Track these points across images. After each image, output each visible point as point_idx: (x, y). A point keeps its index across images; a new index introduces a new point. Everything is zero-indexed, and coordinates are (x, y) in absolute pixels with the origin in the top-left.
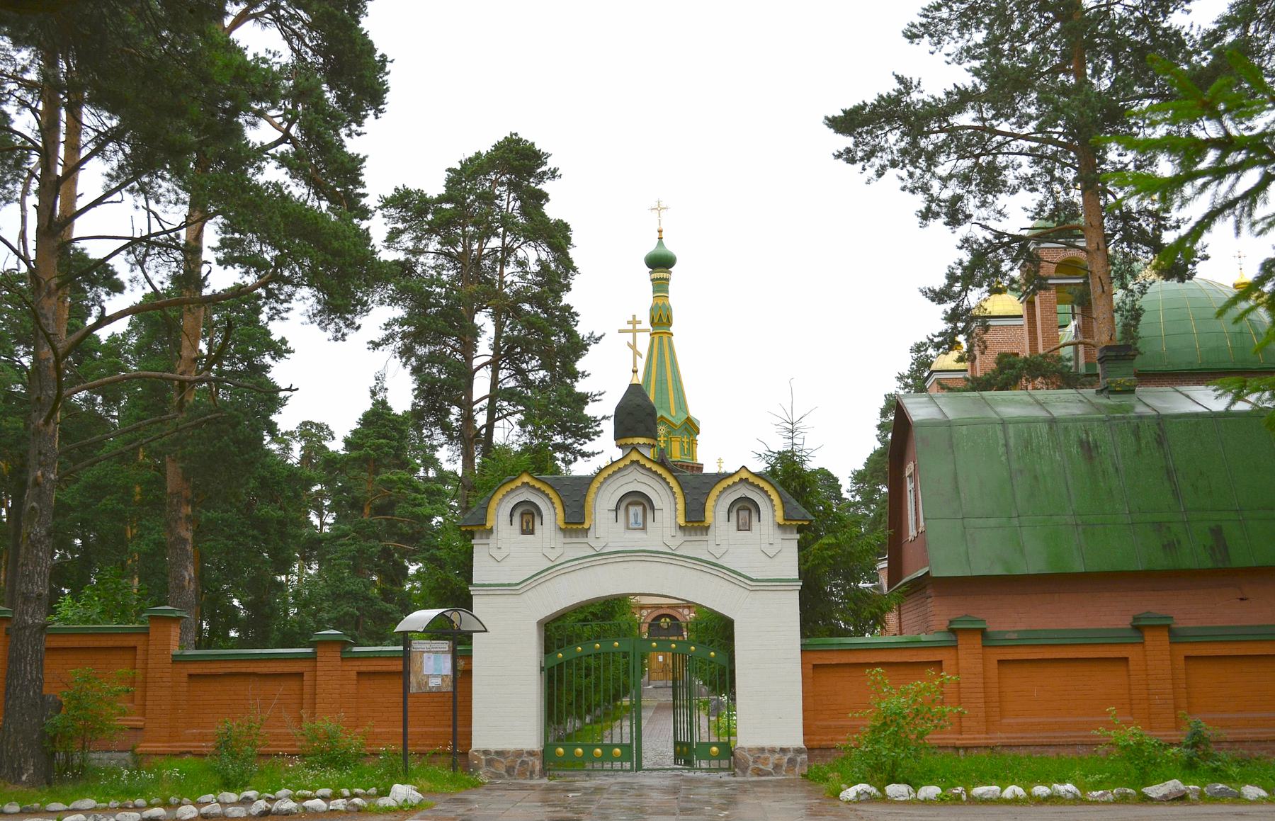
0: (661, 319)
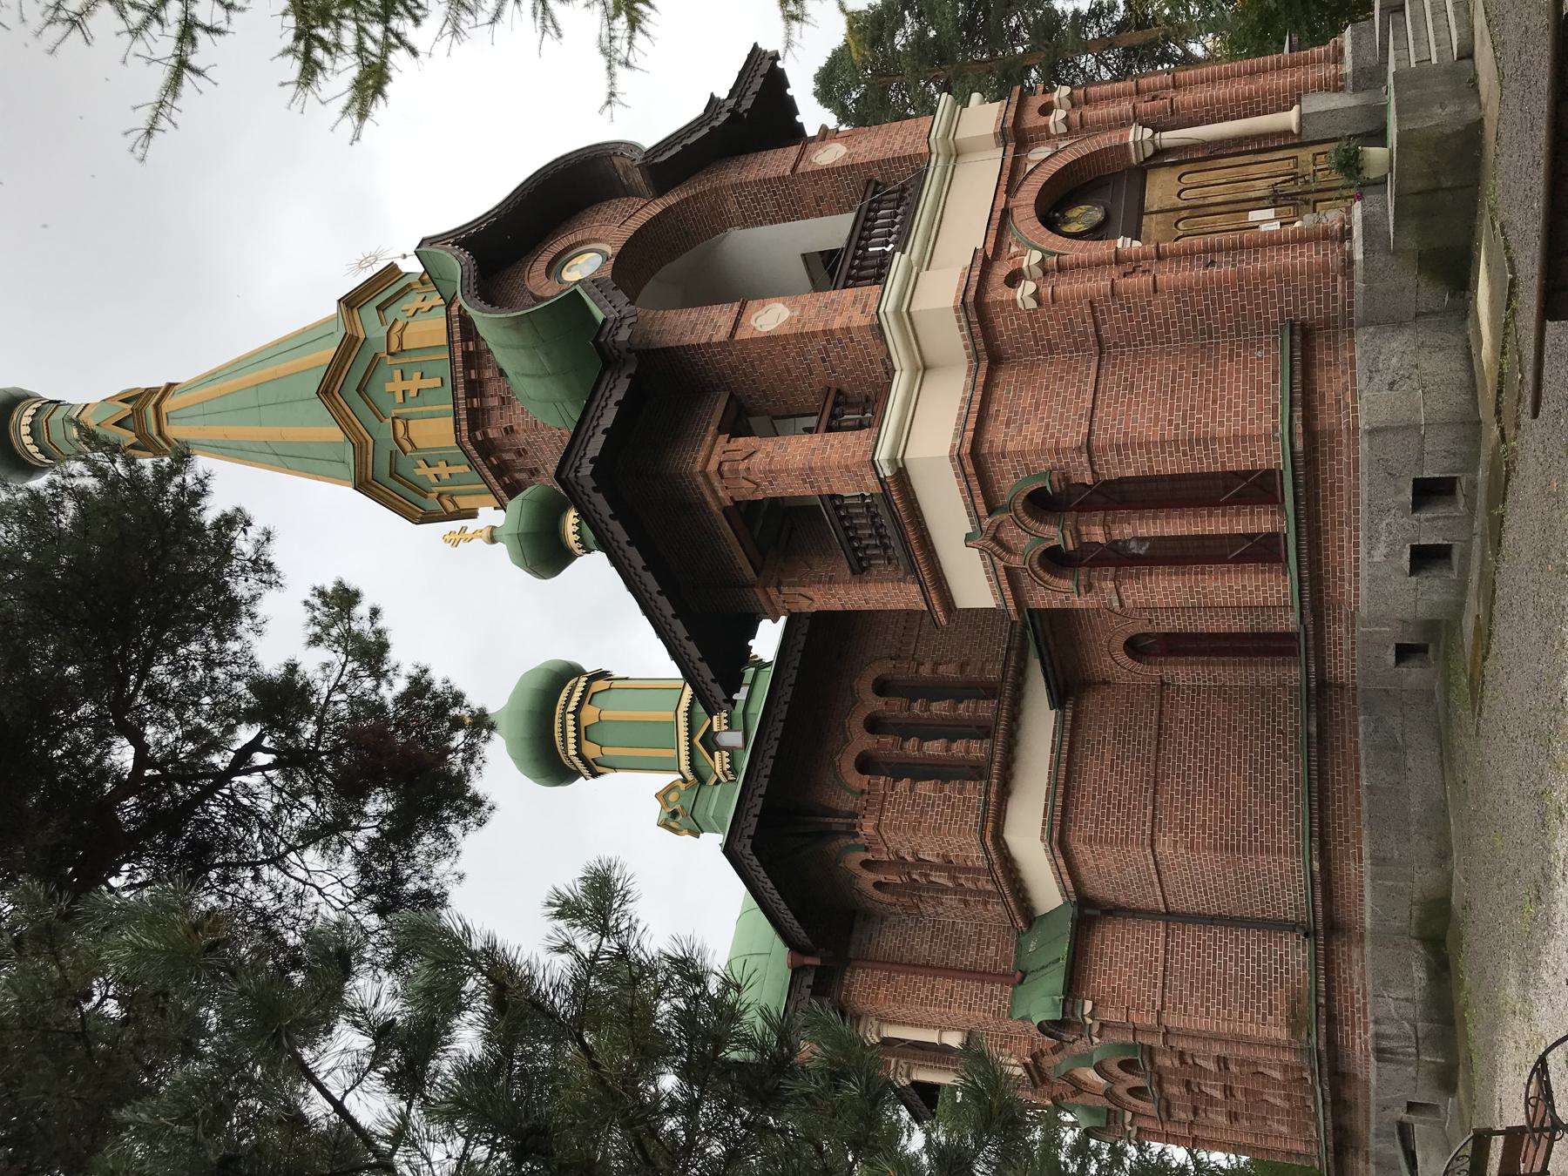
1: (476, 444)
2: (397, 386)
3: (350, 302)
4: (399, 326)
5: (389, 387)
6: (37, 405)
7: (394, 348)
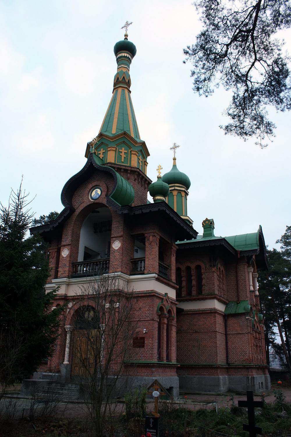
0: (122, 83)
1: (135, 171)
3: (143, 144)
4: (137, 154)
5: (123, 149)
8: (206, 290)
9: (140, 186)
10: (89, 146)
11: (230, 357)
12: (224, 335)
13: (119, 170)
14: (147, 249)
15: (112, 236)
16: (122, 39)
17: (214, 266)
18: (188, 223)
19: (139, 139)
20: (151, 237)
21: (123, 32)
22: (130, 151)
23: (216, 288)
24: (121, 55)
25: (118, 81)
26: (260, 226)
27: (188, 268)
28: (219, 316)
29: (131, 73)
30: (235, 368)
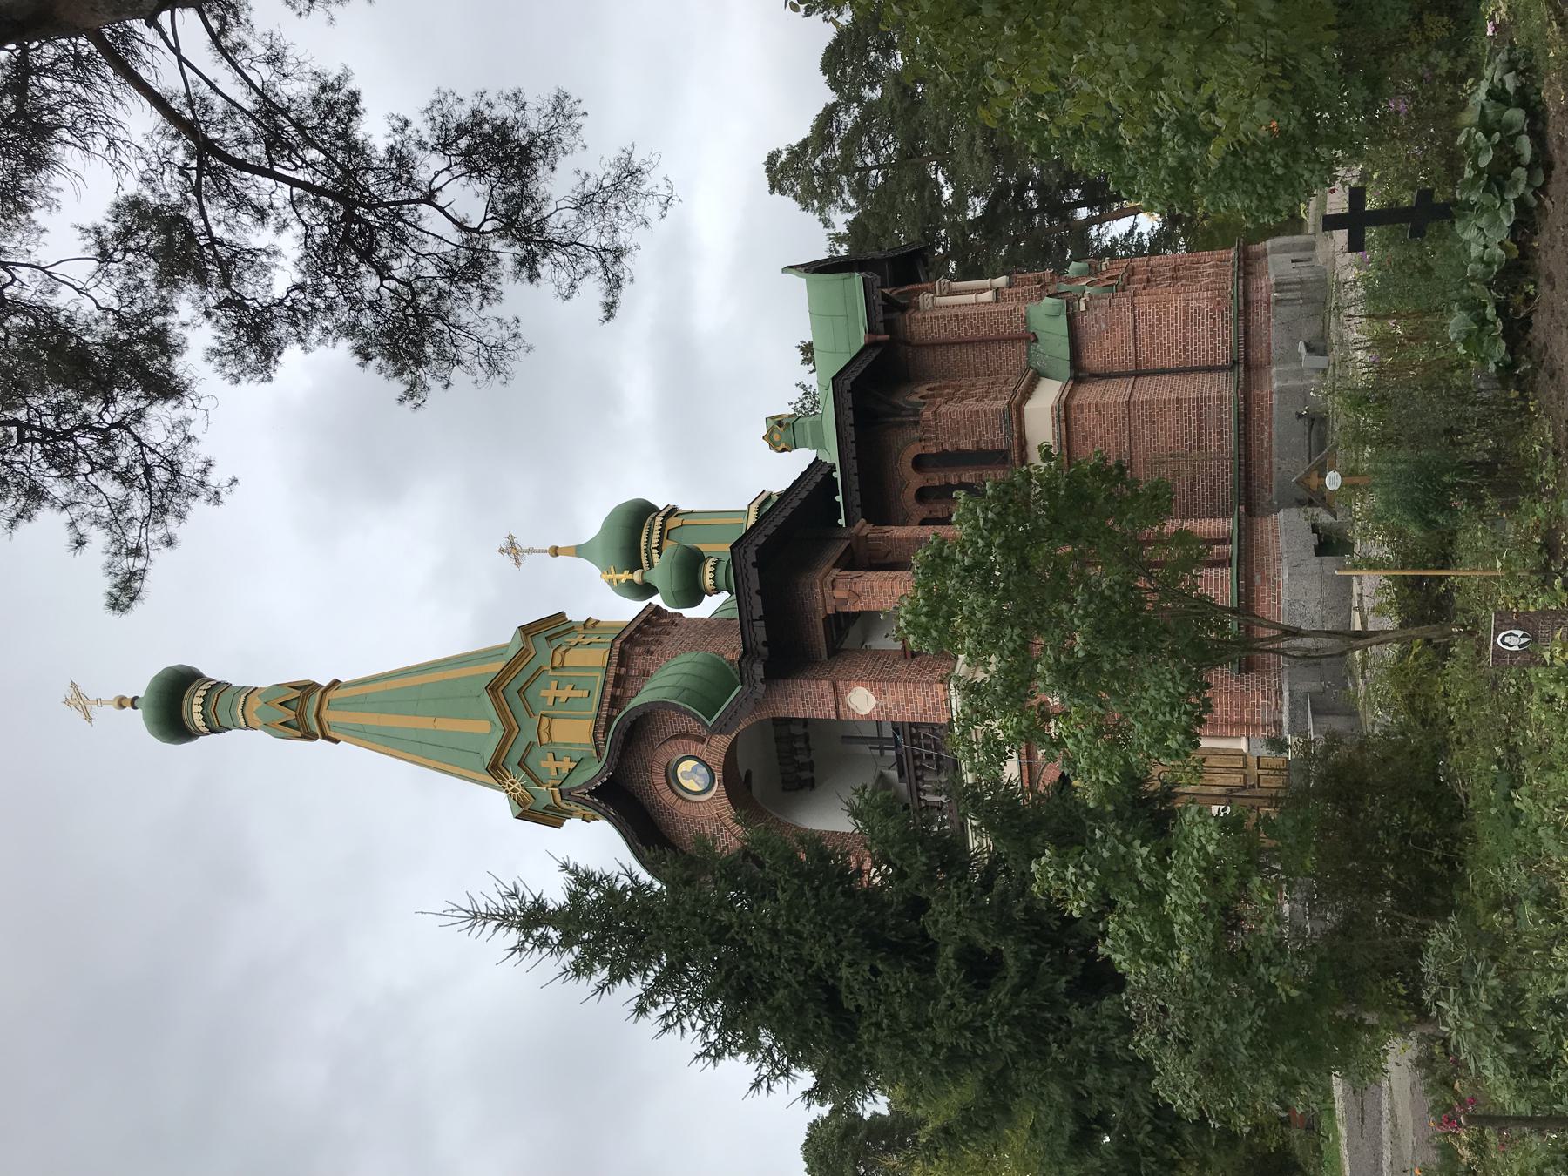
0: (303, 711)
1: (622, 652)
2: (550, 693)
3: (527, 631)
5: (543, 693)
6: (206, 686)
7: (556, 664)
8: (991, 438)
9: (666, 639)
10: (527, 812)
11: (1209, 362)
12: (1140, 380)
13: (616, 702)
14: (874, 607)
15: (833, 717)
16: (136, 719)
17: (917, 413)
18: (770, 507)
19: (506, 646)
20: (838, 594)
21: (108, 715)
22: (551, 673)
23: (986, 405)
24: (197, 717)
25: (295, 723)
26: (784, 270)
27: (922, 495)
28: (1077, 397)
29: (264, 682)
30: (1246, 347)
